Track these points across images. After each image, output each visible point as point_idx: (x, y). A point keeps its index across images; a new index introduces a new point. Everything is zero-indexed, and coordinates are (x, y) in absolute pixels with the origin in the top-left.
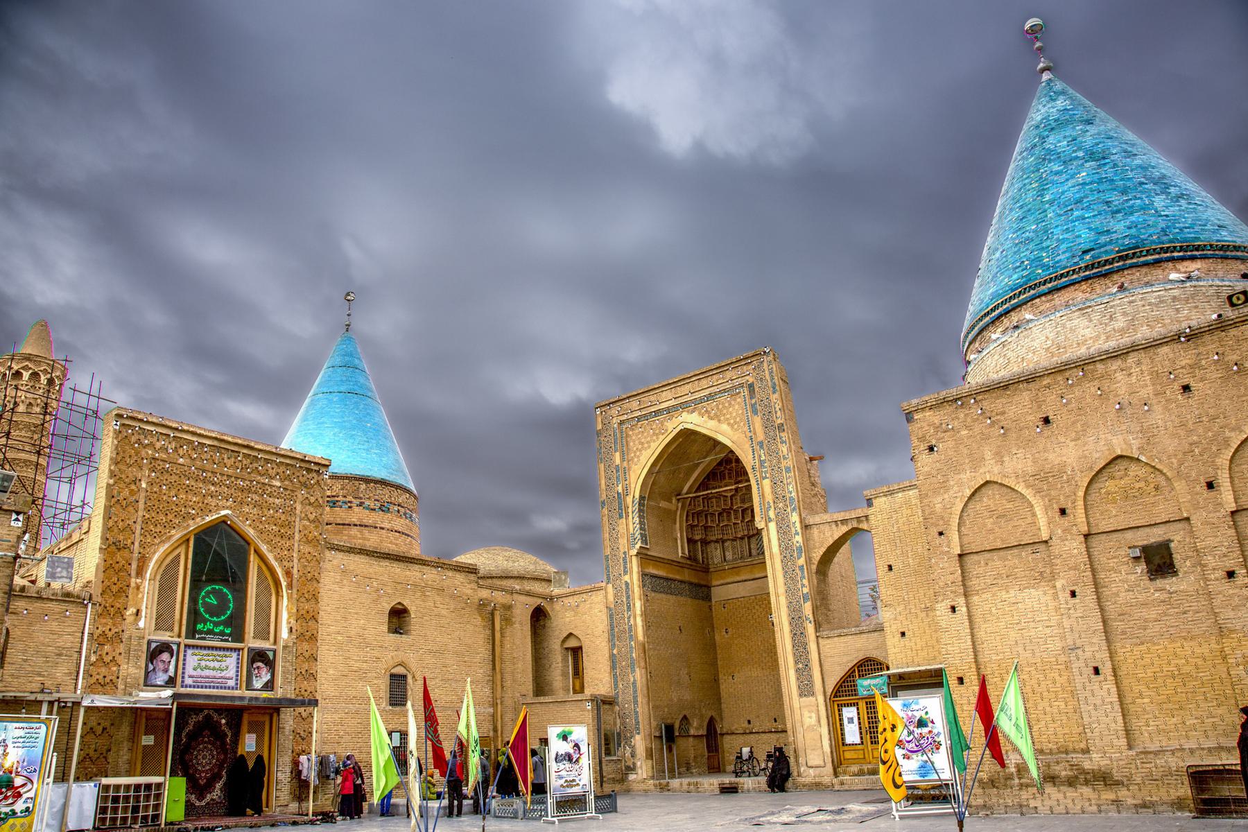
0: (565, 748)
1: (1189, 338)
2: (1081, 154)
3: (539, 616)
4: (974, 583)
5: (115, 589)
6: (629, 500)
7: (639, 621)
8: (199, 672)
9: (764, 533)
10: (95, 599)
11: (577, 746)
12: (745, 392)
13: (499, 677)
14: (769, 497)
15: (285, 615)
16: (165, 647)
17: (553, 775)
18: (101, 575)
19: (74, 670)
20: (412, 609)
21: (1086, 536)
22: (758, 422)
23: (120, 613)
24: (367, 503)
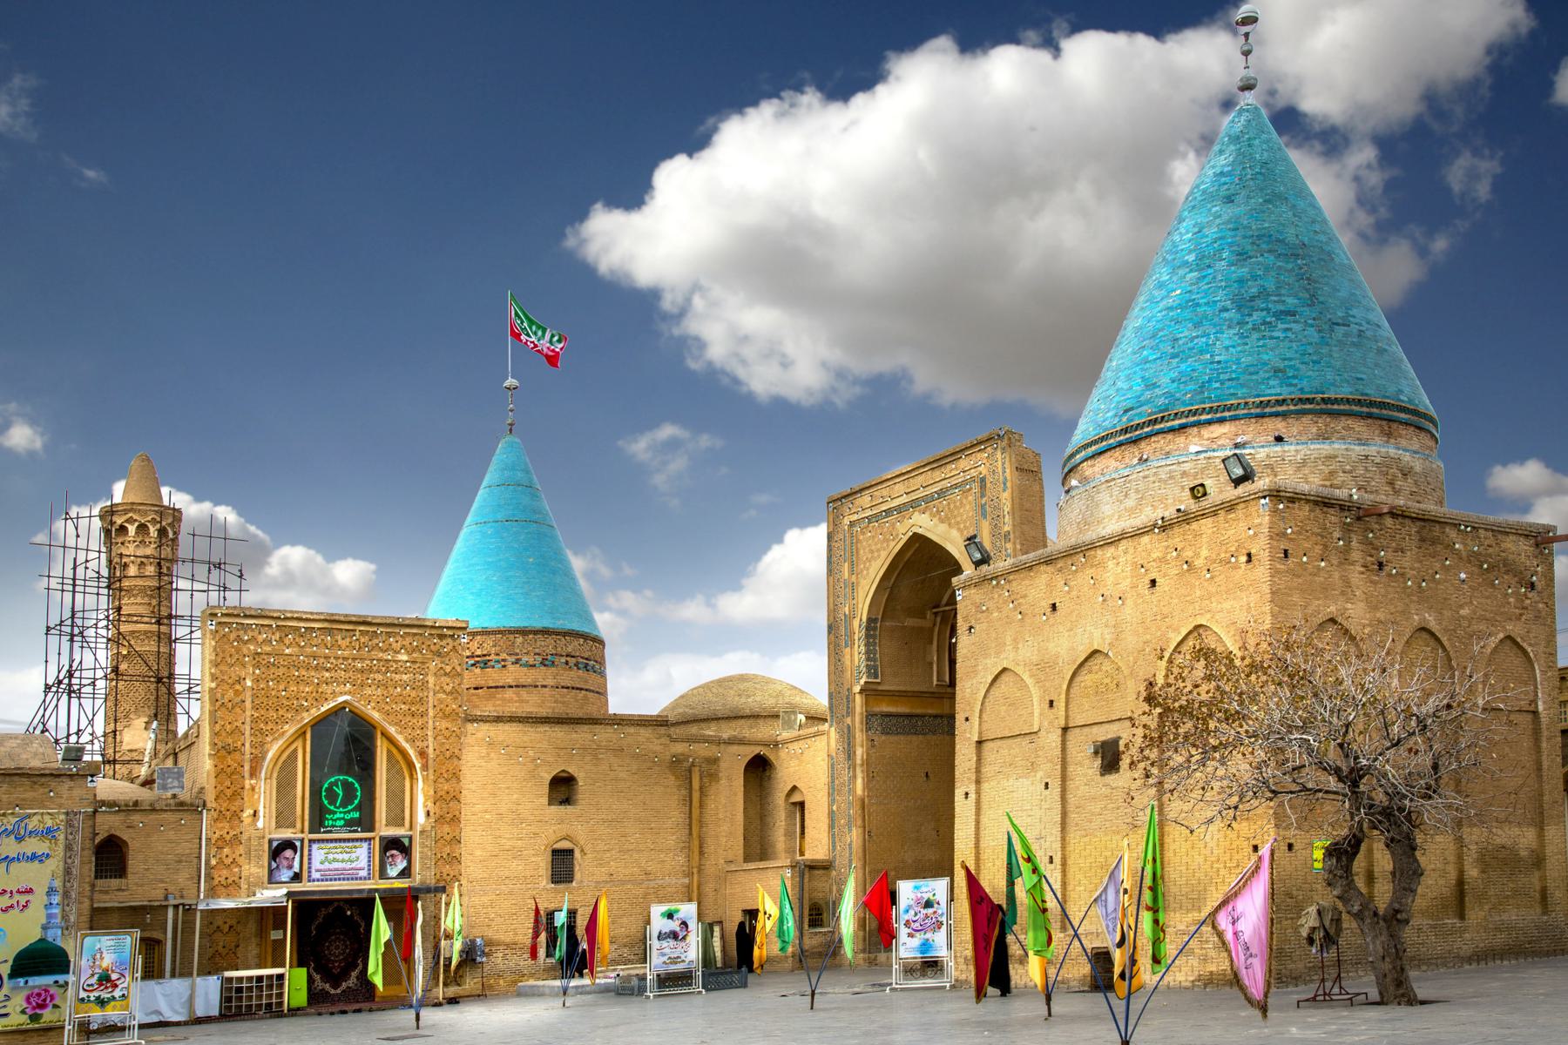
0: (674, 925)
1: (1163, 529)
3: (759, 768)
4: (987, 770)
5: (229, 793)
6: (856, 623)
8: (327, 866)
10: (209, 805)
11: (684, 924)
12: (976, 488)
13: (696, 843)
15: (420, 799)
16: (288, 844)
17: (655, 953)
19: (195, 874)
23: (237, 815)
24: (525, 659)
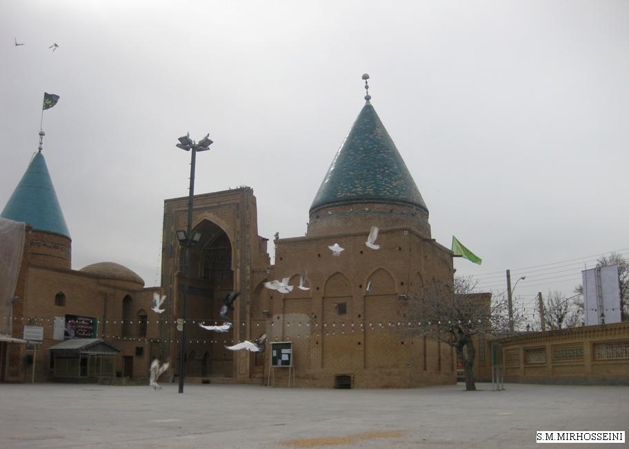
2: (361, 149)
7: (175, 306)
14: (239, 258)
20: (66, 294)
21: (323, 298)
22: (238, 221)
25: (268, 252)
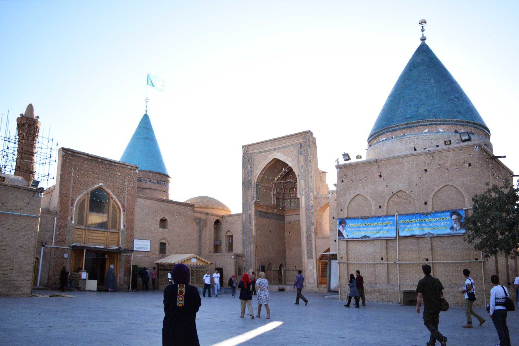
5: (64, 210)
6: (253, 183)
7: (254, 228)
9: (300, 199)
18: (59, 205)
22: (302, 158)
23: (66, 218)
25: (327, 183)
